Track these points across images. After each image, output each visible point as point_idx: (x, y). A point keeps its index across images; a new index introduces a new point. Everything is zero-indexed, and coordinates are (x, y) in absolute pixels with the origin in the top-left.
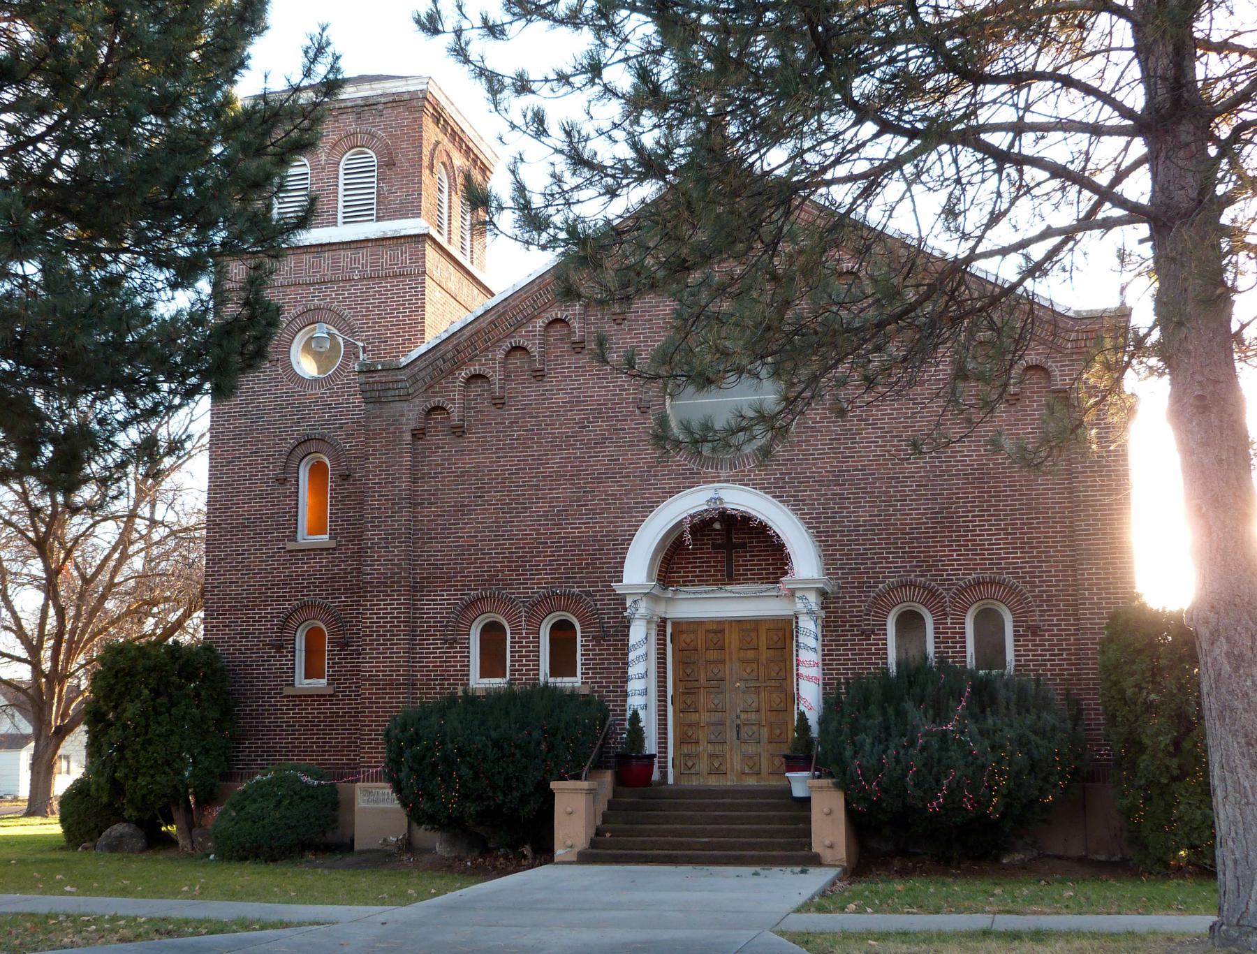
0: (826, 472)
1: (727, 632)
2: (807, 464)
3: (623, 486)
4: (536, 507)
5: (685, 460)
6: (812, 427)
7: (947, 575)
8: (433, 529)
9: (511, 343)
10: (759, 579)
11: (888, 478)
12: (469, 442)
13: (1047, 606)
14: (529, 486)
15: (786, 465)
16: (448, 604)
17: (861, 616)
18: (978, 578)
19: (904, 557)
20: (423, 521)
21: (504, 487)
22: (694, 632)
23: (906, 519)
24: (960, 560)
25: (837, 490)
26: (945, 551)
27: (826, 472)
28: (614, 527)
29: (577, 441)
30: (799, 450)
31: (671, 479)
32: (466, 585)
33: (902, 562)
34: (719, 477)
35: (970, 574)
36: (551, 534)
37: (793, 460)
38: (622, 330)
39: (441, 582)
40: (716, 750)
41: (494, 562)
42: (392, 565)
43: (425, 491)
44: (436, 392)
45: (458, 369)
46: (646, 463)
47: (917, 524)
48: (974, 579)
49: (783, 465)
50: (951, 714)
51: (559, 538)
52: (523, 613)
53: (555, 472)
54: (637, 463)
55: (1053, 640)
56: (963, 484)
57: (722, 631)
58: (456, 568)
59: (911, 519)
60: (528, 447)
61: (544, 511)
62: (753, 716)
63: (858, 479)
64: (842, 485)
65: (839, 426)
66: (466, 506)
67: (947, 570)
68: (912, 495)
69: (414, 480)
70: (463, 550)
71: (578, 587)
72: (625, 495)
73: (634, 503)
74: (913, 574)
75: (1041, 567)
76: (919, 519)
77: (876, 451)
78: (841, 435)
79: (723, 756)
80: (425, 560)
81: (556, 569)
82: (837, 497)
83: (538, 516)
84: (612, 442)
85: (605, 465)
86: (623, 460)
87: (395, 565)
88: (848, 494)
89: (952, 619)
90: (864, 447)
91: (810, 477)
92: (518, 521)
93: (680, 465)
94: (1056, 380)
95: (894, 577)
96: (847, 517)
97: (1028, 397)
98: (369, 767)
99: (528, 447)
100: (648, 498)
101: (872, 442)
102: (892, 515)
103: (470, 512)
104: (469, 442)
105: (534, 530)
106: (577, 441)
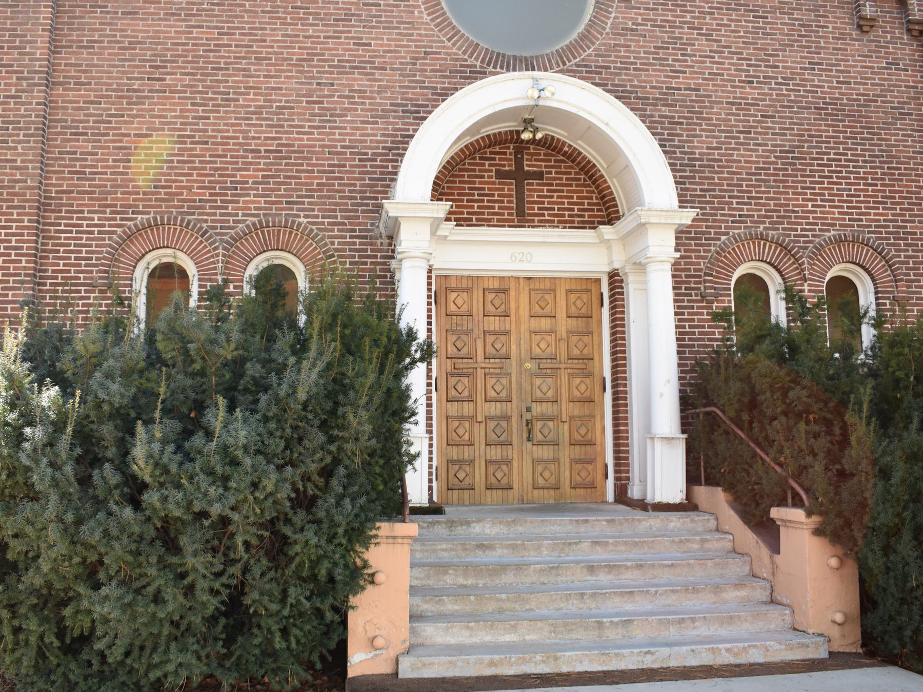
0: (652, 87)
1: (512, 293)
2: (626, 75)
4: (244, 100)
5: (464, 53)
6: (632, 30)
7: (802, 230)
8: (81, 121)
10: (559, 222)
11: (728, 103)
13: (915, 275)
15: (601, 73)
16: (100, 232)
17: (700, 277)
18: (840, 236)
19: (750, 204)
20: (66, 108)
21: (197, 68)
22: (468, 291)
23: (751, 156)
24: (815, 212)
25: (665, 111)
26: (798, 200)
27: (652, 87)
29: (310, 14)
30: (616, 57)
31: (445, 77)
32: (130, 206)
33: (748, 210)
35: (829, 231)
36: (266, 138)
37: (609, 68)
39: (90, 199)
40: (494, 453)
41: (177, 174)
43: (71, 65)
46: (408, 52)
47: (764, 163)
48: (834, 236)
49: (597, 73)
50: (86, 429)
51: (278, 145)
52: (221, 251)
53: (275, 53)
54: (396, 52)
56: (815, 119)
57: (505, 291)
59: (757, 156)
60: (236, 17)
61: (256, 107)
62: (547, 409)
63: (691, 101)
64: (671, 106)
65: (666, 32)
66: (135, 91)
67: (801, 224)
68: (756, 127)
69: (54, 48)
71: (306, 217)
72: (379, 92)
73: (392, 105)
74: (762, 226)
75: (906, 227)
76: (768, 157)
77: (712, 68)
78: (668, 43)
79: (509, 463)
80: (65, 166)
81: (272, 190)
82: (666, 120)
83: (247, 113)
84: (361, 21)
85: (351, 50)
86: (376, 45)
87: (17, 168)
88: (679, 117)
89: (809, 285)
90: (696, 62)
91: (631, 92)
93: (457, 60)
94: (913, 10)
95: (740, 228)
96: (678, 147)
97: (881, 27)
99: (236, 17)
100: (411, 99)
101: (707, 57)
102: (734, 149)
105: (240, 132)
106: (310, 14)
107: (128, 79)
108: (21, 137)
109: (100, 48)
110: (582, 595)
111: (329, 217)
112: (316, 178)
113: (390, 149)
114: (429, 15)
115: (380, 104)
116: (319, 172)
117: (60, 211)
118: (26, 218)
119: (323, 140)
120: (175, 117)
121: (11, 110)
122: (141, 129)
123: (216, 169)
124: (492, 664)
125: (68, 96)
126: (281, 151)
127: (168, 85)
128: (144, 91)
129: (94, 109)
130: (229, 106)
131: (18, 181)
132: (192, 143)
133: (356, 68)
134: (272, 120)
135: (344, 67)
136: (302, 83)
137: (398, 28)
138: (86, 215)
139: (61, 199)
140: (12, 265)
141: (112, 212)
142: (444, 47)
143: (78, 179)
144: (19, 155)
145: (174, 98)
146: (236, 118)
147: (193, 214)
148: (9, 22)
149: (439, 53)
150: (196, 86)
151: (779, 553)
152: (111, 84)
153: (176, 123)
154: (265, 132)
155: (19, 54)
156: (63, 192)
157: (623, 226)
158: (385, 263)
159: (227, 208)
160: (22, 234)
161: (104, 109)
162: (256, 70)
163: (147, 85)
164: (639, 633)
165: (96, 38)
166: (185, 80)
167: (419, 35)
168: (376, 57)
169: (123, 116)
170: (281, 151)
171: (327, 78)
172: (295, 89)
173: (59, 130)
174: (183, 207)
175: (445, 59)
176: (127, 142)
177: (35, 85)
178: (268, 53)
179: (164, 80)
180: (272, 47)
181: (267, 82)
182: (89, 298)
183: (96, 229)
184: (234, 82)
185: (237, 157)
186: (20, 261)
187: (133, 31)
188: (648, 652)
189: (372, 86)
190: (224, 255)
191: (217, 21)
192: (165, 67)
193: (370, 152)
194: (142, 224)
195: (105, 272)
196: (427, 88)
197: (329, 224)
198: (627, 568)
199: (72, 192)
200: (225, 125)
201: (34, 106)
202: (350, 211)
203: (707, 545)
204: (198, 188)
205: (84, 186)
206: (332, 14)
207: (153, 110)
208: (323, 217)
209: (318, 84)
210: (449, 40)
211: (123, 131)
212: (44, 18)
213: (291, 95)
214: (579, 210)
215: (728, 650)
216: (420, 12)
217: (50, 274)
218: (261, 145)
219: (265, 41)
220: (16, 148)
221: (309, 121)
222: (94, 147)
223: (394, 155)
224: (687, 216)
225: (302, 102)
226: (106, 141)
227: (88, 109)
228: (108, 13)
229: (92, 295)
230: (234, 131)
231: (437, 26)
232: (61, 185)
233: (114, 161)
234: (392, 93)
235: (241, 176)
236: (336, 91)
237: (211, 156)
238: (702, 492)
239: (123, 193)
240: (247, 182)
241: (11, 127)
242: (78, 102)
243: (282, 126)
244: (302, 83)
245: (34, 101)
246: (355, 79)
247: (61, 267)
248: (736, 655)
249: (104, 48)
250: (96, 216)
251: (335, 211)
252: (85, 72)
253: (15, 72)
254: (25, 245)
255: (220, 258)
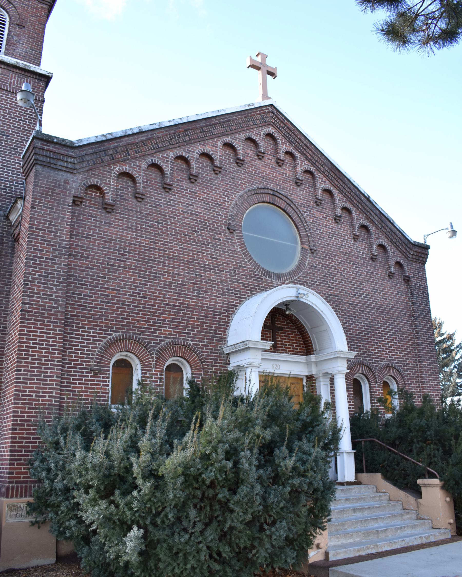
3: (220, 276)
5: (255, 268)
8: (84, 278)
9: (152, 160)
10: (289, 351)
12: (115, 219)
14: (158, 261)
16: (94, 340)
20: (76, 269)
28: (215, 302)
31: (247, 279)
32: (109, 327)
34: (272, 283)
36: (174, 299)
38: (217, 178)
39: (89, 321)
42: (50, 299)
43: (79, 246)
44: (96, 175)
45: (114, 164)
52: (154, 355)
55: (32, 367)
58: (102, 312)
60: (159, 235)
61: (169, 282)
66: (112, 265)
70: (108, 299)
71: (192, 341)
72: (221, 282)
80: (76, 301)
81: (177, 326)
83: (165, 285)
92: (150, 285)
93: (252, 271)
98: (16, 482)
99: (159, 235)
100: (234, 288)
103: (114, 271)
104: (115, 219)
106: (192, 239)
107: (108, 258)
108: (55, 283)
109: (93, 239)
110: (362, 520)
111: (201, 342)
112: (196, 321)
113: (227, 311)
114: (240, 248)
115: (222, 288)
116: (197, 318)
117: (73, 326)
118: (58, 329)
119: (198, 303)
120: (131, 282)
121: (49, 266)
122: (114, 286)
123: (151, 312)
124: (358, 551)
125: (77, 262)
126: (180, 306)
127: (127, 265)
128: (116, 266)
129: (91, 272)
130: (156, 280)
131: (54, 307)
132: (139, 297)
133: (211, 269)
134: (176, 290)
135: (206, 268)
136: (189, 273)
137: (228, 252)
138: (86, 330)
139: (73, 319)
140: (50, 355)
141: (100, 330)
142: (246, 264)
143: (82, 309)
144: (54, 292)
145: (130, 272)
146: (160, 287)
147: (140, 335)
148: (48, 216)
149: (245, 267)
150: (140, 267)
151: (421, 498)
152: (99, 260)
153: (131, 285)
154: (173, 296)
155: (54, 235)
156: (74, 316)
157: (313, 358)
158: (225, 367)
159: (156, 333)
160: (56, 338)
161: (96, 273)
162: (168, 264)
163: (117, 263)
164: (390, 535)
165: (91, 233)
166: (135, 263)
167: (237, 257)
168: (219, 265)
169: (105, 278)
170: (180, 306)
171: (199, 272)
172: (186, 276)
173: (72, 281)
174: (135, 330)
175: (247, 270)
176: (107, 292)
177: (63, 254)
178: (173, 256)
179: (126, 262)
180: (175, 253)
181: (173, 270)
182: (88, 376)
183: (92, 338)
184: (158, 268)
185: (161, 307)
186: (55, 353)
187: (110, 233)
188: (403, 540)
189: (218, 279)
190: (156, 358)
191: (150, 235)
192: (126, 255)
193: (218, 311)
194: (117, 337)
195: (98, 362)
196: (240, 283)
197: (202, 345)
198: (365, 509)
199: (79, 316)
200: (155, 289)
201: (62, 266)
202: (211, 339)
203: (381, 498)
204: (142, 321)
205: (85, 313)
206: (201, 241)
207: (120, 277)
208: (199, 342)
209: (196, 275)
210: (249, 261)
211: (105, 286)
212: (68, 218)
213: (184, 279)
214: (27, 331)
215: (425, 537)
216: (237, 246)
217: (67, 361)
218: (171, 302)
219: (172, 249)
220: (52, 289)
221: (192, 292)
222: (90, 293)
223: (228, 314)
224: (352, 355)
225: (189, 283)
226: (97, 290)
227: (87, 271)
228: (97, 221)
229: (90, 375)
230: (159, 293)
231: (244, 254)
232: (73, 312)
233: (101, 302)
234: (227, 283)
235: (163, 317)
236: (204, 279)
237: (148, 305)
238: (364, 476)
239: (106, 320)
240: (165, 321)
241: (49, 276)
242: (82, 267)
243: (180, 294)
244: (189, 273)
245: (62, 263)
246: (211, 275)
247: (73, 358)
248: (427, 539)
249: (96, 240)
250: (92, 331)
251: (204, 339)
252: (86, 251)
253: (52, 245)
254: (57, 344)
255: (154, 359)
